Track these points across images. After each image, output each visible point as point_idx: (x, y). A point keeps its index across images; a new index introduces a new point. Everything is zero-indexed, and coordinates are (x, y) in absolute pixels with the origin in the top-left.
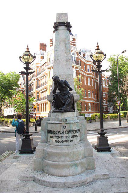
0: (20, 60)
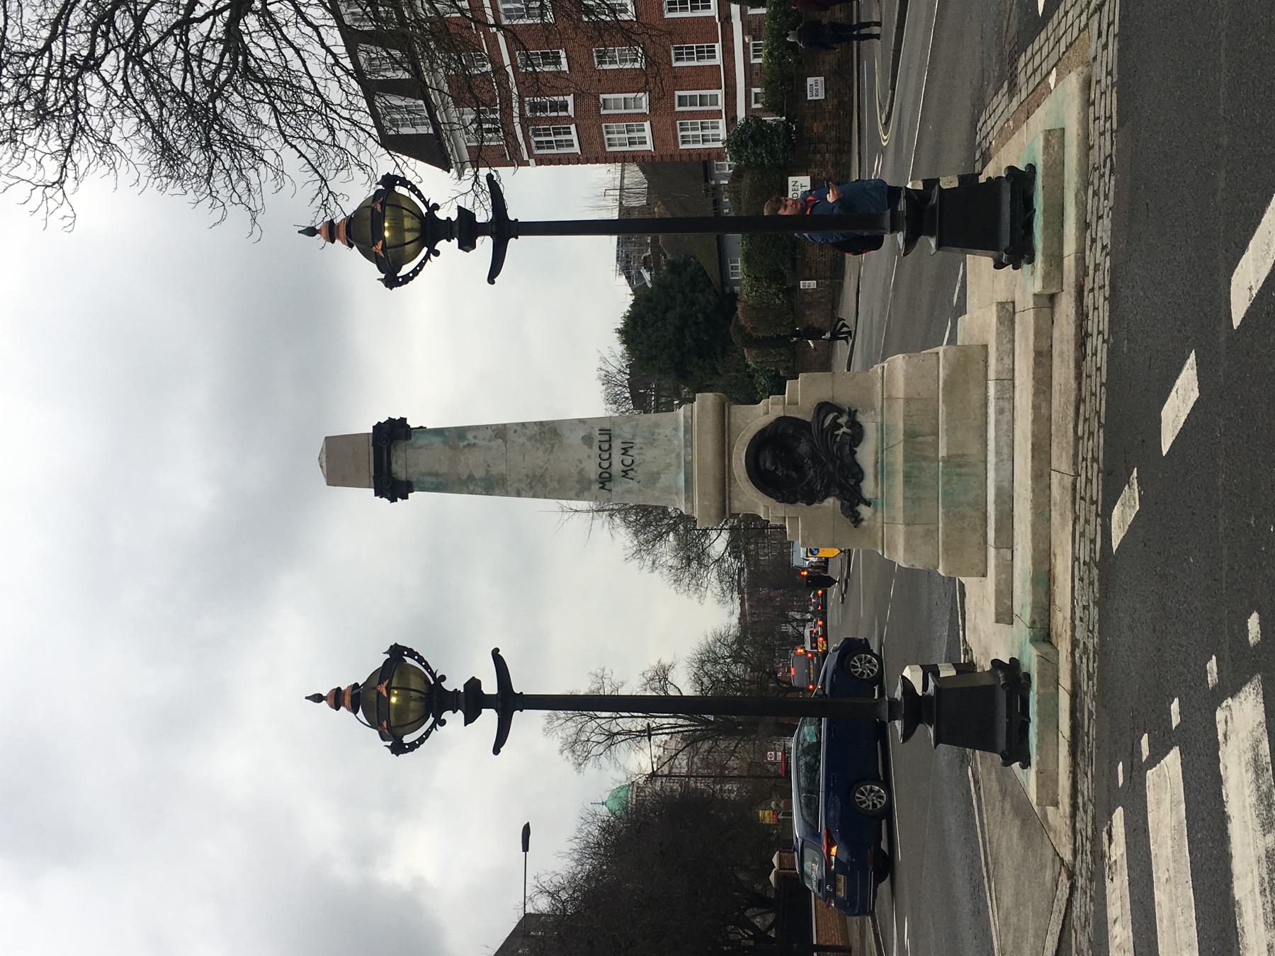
0: (413, 746)
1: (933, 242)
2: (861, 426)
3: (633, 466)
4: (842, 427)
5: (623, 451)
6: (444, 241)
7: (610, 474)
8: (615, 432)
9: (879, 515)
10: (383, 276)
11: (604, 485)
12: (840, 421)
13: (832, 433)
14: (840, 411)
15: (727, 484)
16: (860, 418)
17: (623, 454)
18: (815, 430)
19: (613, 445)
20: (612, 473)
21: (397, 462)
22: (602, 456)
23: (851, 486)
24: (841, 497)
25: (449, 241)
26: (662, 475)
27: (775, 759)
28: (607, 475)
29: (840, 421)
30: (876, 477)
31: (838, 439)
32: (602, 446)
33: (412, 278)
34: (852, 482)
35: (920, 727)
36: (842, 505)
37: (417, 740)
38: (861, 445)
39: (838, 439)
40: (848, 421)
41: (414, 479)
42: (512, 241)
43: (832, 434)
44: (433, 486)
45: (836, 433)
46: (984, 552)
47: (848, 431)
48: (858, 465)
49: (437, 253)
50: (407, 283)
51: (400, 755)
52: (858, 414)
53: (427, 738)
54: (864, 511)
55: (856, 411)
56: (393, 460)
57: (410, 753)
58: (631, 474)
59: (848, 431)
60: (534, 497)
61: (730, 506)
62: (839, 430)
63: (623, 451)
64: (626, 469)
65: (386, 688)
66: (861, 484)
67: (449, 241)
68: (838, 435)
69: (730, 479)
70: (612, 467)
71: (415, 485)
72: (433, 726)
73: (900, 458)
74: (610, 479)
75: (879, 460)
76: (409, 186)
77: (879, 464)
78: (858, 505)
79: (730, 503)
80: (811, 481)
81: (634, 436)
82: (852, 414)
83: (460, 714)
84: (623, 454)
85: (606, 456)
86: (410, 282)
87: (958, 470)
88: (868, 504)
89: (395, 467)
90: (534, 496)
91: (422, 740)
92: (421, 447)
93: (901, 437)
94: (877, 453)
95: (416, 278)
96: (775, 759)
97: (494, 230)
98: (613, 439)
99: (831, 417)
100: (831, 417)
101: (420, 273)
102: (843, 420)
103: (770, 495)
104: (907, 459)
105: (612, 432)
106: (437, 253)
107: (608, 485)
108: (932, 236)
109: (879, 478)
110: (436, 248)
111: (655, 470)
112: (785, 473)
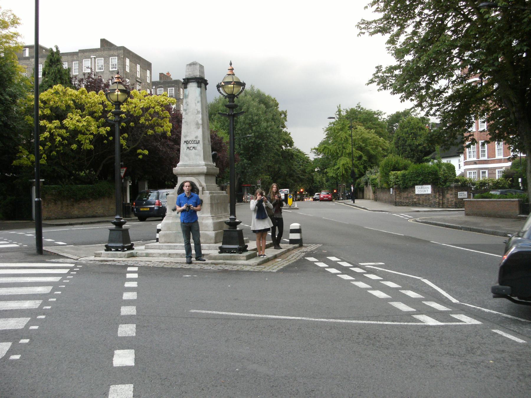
0: (219, 90)
56: (193, 83)
58: (188, 149)
74: (187, 143)
85: (193, 142)
107: (185, 143)
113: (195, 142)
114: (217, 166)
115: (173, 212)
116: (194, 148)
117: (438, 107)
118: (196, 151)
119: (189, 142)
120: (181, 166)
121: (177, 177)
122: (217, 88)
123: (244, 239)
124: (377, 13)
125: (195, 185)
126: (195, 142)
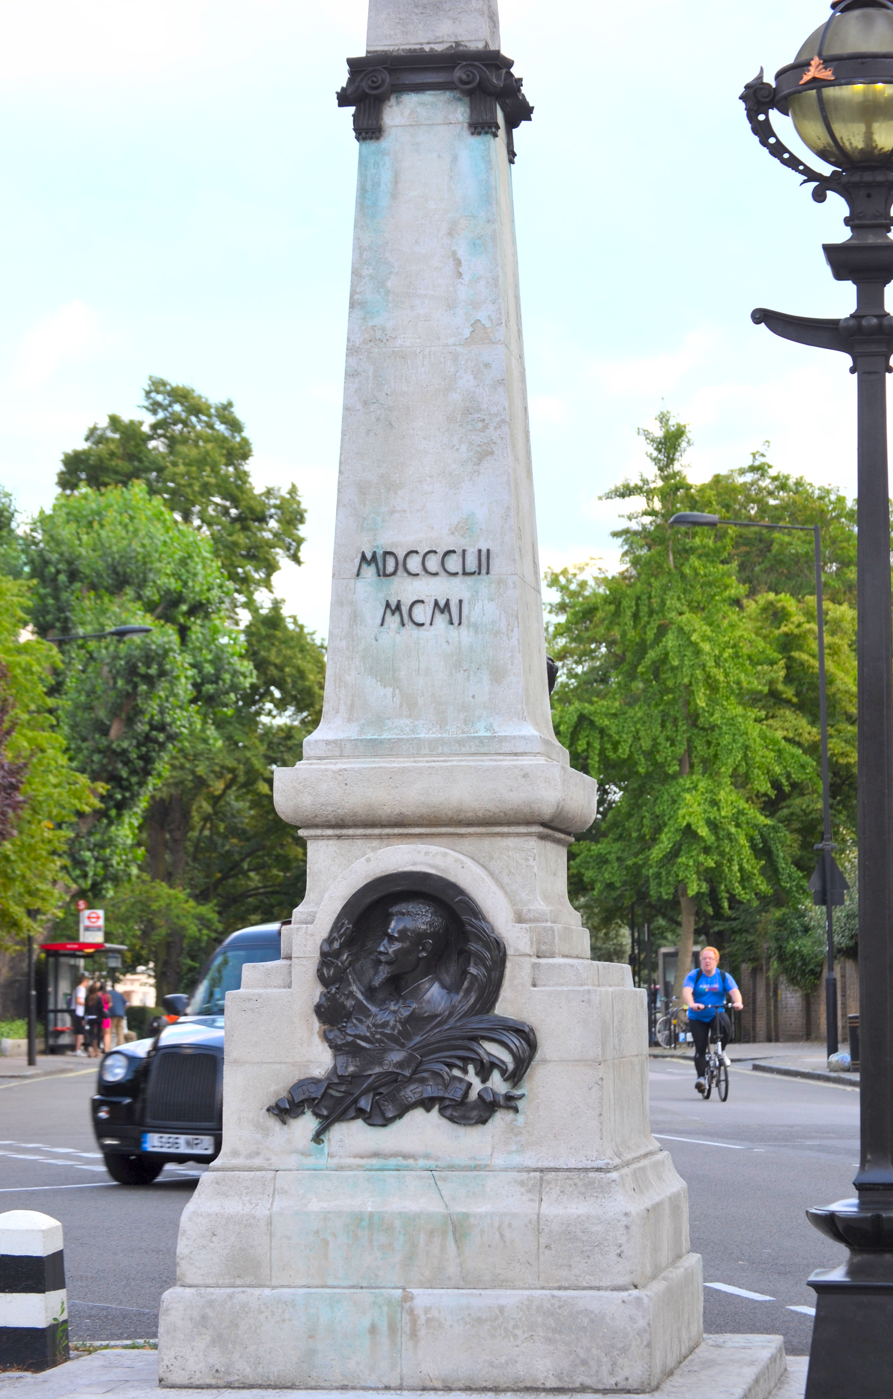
0: (763, 131)
1: (837, 1275)
2: (484, 1122)
3: (409, 626)
4: (484, 1081)
5: (442, 603)
6: (846, 212)
7: (394, 573)
8: (483, 584)
9: (293, 1160)
10: (770, 79)
11: (369, 563)
12: (496, 1076)
13: (472, 1060)
14: (515, 1077)
15: (369, 831)
16: (500, 1119)
17: (436, 603)
18: (475, 1023)
19: (456, 581)
20: (396, 580)
21: (423, 104)
22: (432, 555)
23: (356, 1101)
24: (336, 1079)
25: (847, 221)
26: (390, 690)
27: (87, 929)
28: (390, 568)
29: (496, 1076)
30: (376, 1155)
31: (456, 1072)
32: (453, 556)
33: (764, 143)
34: (365, 1103)
35: (842, 1252)
36: (315, 1081)
37: (778, 141)
38: (445, 1122)
39: (456, 1072)
40: (494, 1094)
41: (386, 143)
42: (845, 360)
43: (466, 1060)
44: (369, 186)
45: (471, 1068)
46: (209, 1381)
47: (473, 1095)
48: (400, 1116)
49: (819, 196)
50: (755, 131)
51: (742, 105)
52: (509, 1116)
53: (784, 162)
54: (307, 1123)
55: (516, 1110)
56: (428, 97)
57: (748, 126)
58: (393, 621)
59: (473, 1095)
60: (346, 408)
61: (497, 834)
62: (477, 1074)
63: (442, 603)
64: (405, 609)
65: (814, 79)
66: (359, 1122)
67: (847, 221)
68: (465, 1072)
69: (380, 837)
70: (410, 579)
71: (372, 145)
72: (810, 175)
73: (411, 1206)
74: (382, 574)
75: (411, 1162)
76: (772, 140)
77: (400, 1161)
78: (317, 1115)
79: (329, 837)
80: (367, 1013)
81: (476, 627)
82: (510, 1103)
83: (842, 235)
84: (436, 603)
85: (433, 564)
86: (756, 139)
87: (384, 1327)
88: (318, 1138)
89: (411, 100)
90: (347, 409)
91: (778, 150)
92: (455, 159)
93: (459, 1208)
94: (427, 1156)
95: (765, 151)
96: (87, 929)
97: (864, 322)
98: (469, 580)
99: (506, 1057)
100: (506, 1057)
101: (776, 161)
102: (497, 1083)
103: (337, 925)
104: (411, 1220)
105: (483, 576)
106: (819, 196)
107: (369, 572)
108: (850, 1272)
109: (374, 1162)
110: (830, 194)
111: (403, 673)
112: (383, 958)
113: (454, 564)
114: (108, 1026)
115: (274, 1124)
116: (442, 608)
117: (714, 1081)
118: (464, 635)
119: (402, 566)
120: (338, 748)
121: (302, 843)
122: (751, 117)
123: (812, 1311)
124: (290, 486)
125: (473, 909)
126: (454, 564)
